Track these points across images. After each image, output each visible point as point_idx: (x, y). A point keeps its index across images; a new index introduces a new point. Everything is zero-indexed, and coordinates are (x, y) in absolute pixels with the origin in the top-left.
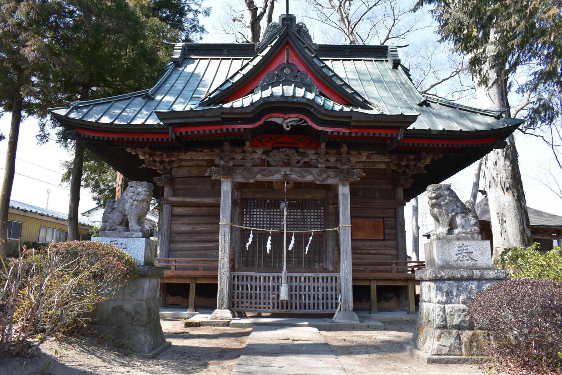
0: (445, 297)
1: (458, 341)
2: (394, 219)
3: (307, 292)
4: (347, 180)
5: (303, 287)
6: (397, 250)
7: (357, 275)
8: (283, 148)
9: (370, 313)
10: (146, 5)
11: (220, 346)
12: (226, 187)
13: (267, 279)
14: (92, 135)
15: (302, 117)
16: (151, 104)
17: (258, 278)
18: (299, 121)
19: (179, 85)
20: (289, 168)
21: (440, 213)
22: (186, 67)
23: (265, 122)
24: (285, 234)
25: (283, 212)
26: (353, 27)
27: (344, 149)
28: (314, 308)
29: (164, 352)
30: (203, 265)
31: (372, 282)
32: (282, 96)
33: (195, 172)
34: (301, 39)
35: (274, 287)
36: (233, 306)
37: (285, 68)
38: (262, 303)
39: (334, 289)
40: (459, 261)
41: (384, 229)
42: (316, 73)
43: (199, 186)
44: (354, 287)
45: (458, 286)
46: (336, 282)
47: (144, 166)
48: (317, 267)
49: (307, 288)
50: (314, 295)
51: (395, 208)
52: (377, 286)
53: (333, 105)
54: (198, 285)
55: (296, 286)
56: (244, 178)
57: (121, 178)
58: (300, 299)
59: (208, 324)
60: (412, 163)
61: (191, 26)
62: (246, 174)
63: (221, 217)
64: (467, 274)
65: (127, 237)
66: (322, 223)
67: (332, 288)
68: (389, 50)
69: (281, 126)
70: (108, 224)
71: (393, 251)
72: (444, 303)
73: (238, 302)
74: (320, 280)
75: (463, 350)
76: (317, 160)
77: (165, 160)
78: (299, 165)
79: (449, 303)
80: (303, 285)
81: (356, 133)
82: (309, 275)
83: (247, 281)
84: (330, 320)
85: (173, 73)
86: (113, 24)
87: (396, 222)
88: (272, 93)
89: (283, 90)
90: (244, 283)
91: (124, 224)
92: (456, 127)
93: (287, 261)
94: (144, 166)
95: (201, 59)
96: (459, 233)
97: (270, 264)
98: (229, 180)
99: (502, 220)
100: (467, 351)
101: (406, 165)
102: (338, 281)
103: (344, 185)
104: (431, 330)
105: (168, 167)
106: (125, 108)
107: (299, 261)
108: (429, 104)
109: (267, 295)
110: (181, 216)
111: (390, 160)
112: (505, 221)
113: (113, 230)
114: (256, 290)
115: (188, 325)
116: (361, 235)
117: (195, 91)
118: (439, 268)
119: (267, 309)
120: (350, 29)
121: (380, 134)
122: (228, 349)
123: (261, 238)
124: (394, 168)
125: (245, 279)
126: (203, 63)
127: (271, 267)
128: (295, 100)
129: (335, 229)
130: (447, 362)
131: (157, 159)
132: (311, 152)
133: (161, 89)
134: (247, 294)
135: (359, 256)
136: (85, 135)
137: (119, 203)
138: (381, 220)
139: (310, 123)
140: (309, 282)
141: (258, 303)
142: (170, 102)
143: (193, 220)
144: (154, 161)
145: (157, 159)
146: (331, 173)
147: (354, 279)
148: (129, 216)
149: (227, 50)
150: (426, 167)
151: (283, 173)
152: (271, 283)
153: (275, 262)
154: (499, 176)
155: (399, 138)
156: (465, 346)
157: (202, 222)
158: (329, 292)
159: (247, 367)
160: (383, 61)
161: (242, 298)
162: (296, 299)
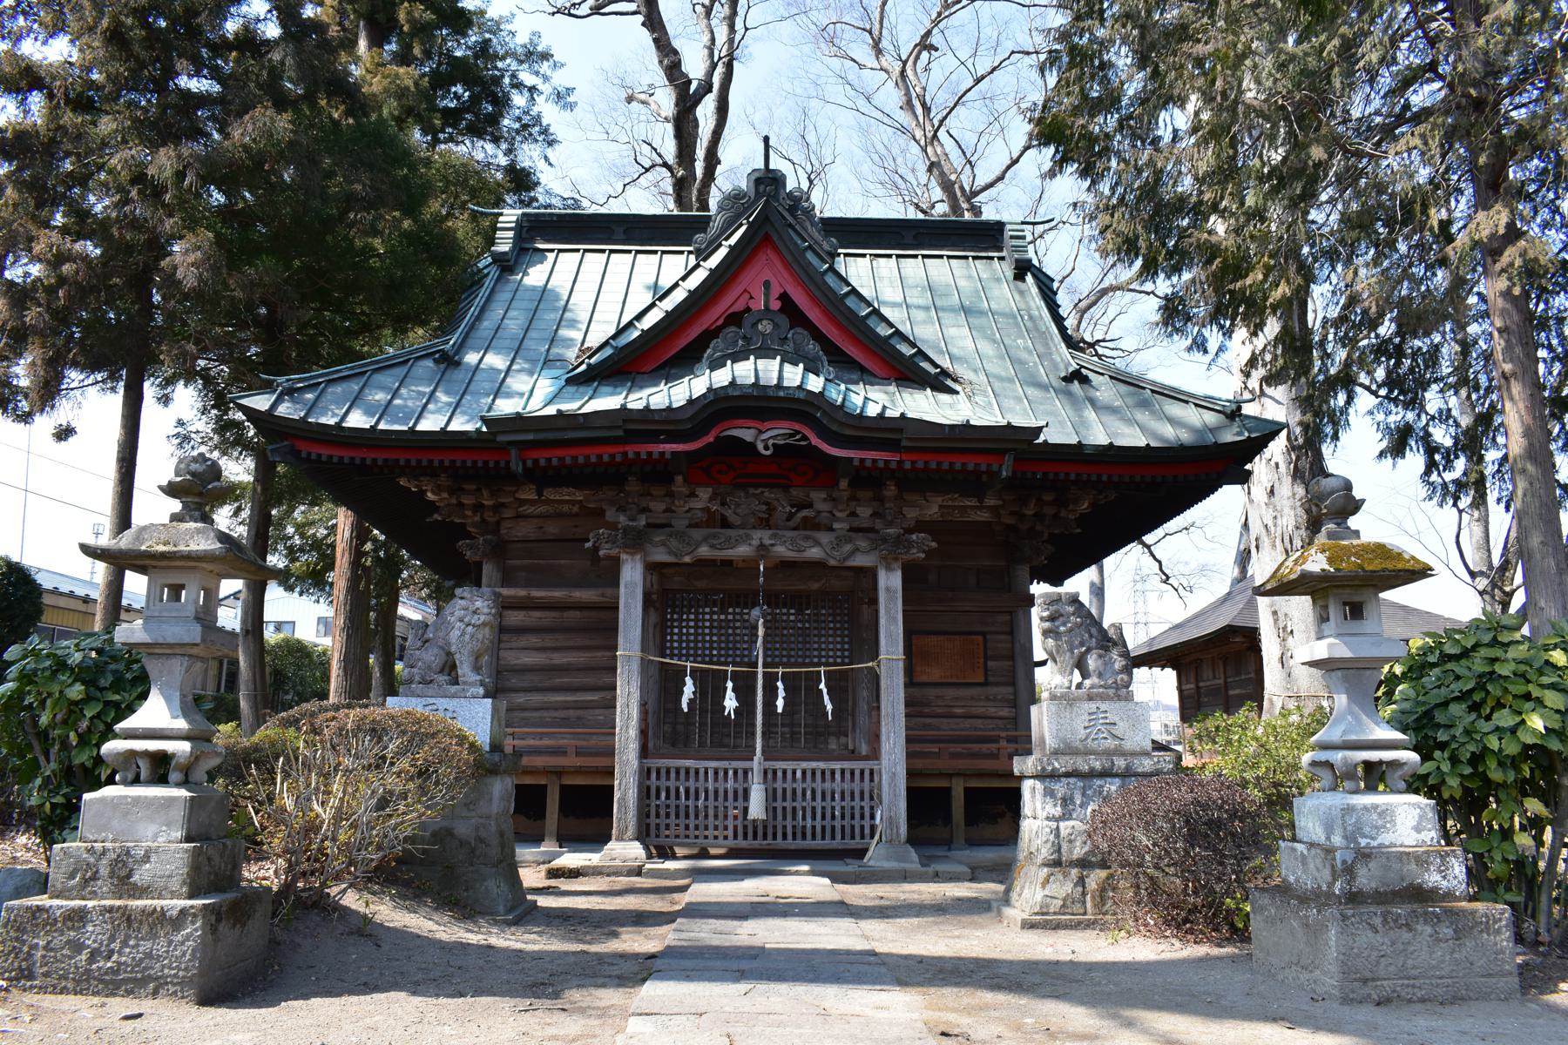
0: (1059, 809)
1: (1080, 889)
2: (1008, 638)
3: (808, 803)
4: (896, 559)
5: (799, 792)
6: (1015, 707)
7: (919, 764)
8: (756, 486)
9: (950, 849)
10: (413, 89)
11: (631, 907)
12: (632, 575)
13: (721, 774)
14: (325, 452)
15: (797, 427)
16: (455, 377)
17: (702, 772)
18: (791, 436)
19: (514, 324)
20: (771, 532)
21: (1058, 647)
22: (525, 273)
23: (717, 438)
24: (760, 676)
25: (756, 628)
26: (936, 123)
27: (891, 490)
28: (823, 838)
29: (529, 917)
30: (574, 742)
31: (955, 780)
32: (756, 385)
33: (553, 529)
34: (797, 227)
35: (736, 792)
36: (648, 835)
37: (760, 320)
38: (711, 827)
39: (867, 796)
40: (1089, 740)
41: (986, 659)
42: (830, 308)
43: (563, 562)
44: (910, 791)
45: (1084, 788)
46: (872, 780)
47: (436, 516)
48: (834, 747)
49: (809, 793)
50: (823, 808)
51: (1011, 613)
52: (967, 790)
53: (864, 403)
54: (566, 791)
55: (784, 790)
56: (670, 553)
57: (349, 522)
58: (794, 818)
59: (596, 872)
60: (1049, 511)
61: (517, 126)
62: (674, 543)
63: (621, 640)
64: (1102, 764)
65: (453, 696)
66: (846, 646)
67: (862, 793)
68: (1008, 234)
69: (752, 446)
70: (415, 670)
71: (1007, 710)
72: (1057, 820)
73: (658, 825)
74: (838, 776)
75: (1089, 905)
76: (831, 512)
77: (485, 502)
78: (792, 524)
79: (1068, 819)
80: (799, 787)
81: (913, 462)
82: (814, 764)
83: (678, 779)
84: (858, 862)
85: (497, 289)
86: (364, 185)
87: (1013, 643)
88: (734, 378)
89: (756, 370)
90: (672, 784)
91: (447, 670)
92: (1133, 438)
93: (764, 733)
94: (436, 516)
95: (560, 251)
96: (1092, 687)
97: (726, 740)
98: (638, 557)
99: (1285, 628)
100: (1095, 906)
101: (1035, 515)
102: (876, 778)
103: (889, 569)
104: (1033, 869)
105: (492, 520)
106: (398, 388)
107: (793, 733)
108: (1087, 377)
109: (721, 809)
110: (521, 630)
111: (1001, 503)
112: (1292, 632)
113: (426, 682)
114: (697, 799)
115: (554, 873)
116: (934, 674)
117: (552, 341)
118: (1051, 753)
119: (721, 841)
120: (929, 127)
121: (963, 464)
122: (650, 912)
123: (710, 688)
124: (1011, 521)
125: (673, 775)
126: (568, 261)
127: (728, 746)
128: (781, 394)
129: (870, 664)
130: (1057, 926)
131: (468, 500)
132: (818, 496)
133: (472, 335)
134: (677, 807)
135: (928, 721)
136: (309, 454)
137: (437, 630)
138: (980, 638)
139: (815, 441)
140: (814, 779)
141: (702, 827)
142: (499, 371)
143: (549, 640)
144: (461, 505)
145: (468, 500)
146: (863, 544)
147: (911, 774)
148: (457, 656)
149: (622, 229)
150: (1082, 519)
151: (755, 542)
152: (730, 784)
153: (738, 735)
154: (1279, 521)
155: (1004, 473)
156: (1093, 897)
157: (571, 643)
158: (857, 803)
159: (692, 934)
160: (992, 258)
161: (668, 815)
162: (784, 818)
